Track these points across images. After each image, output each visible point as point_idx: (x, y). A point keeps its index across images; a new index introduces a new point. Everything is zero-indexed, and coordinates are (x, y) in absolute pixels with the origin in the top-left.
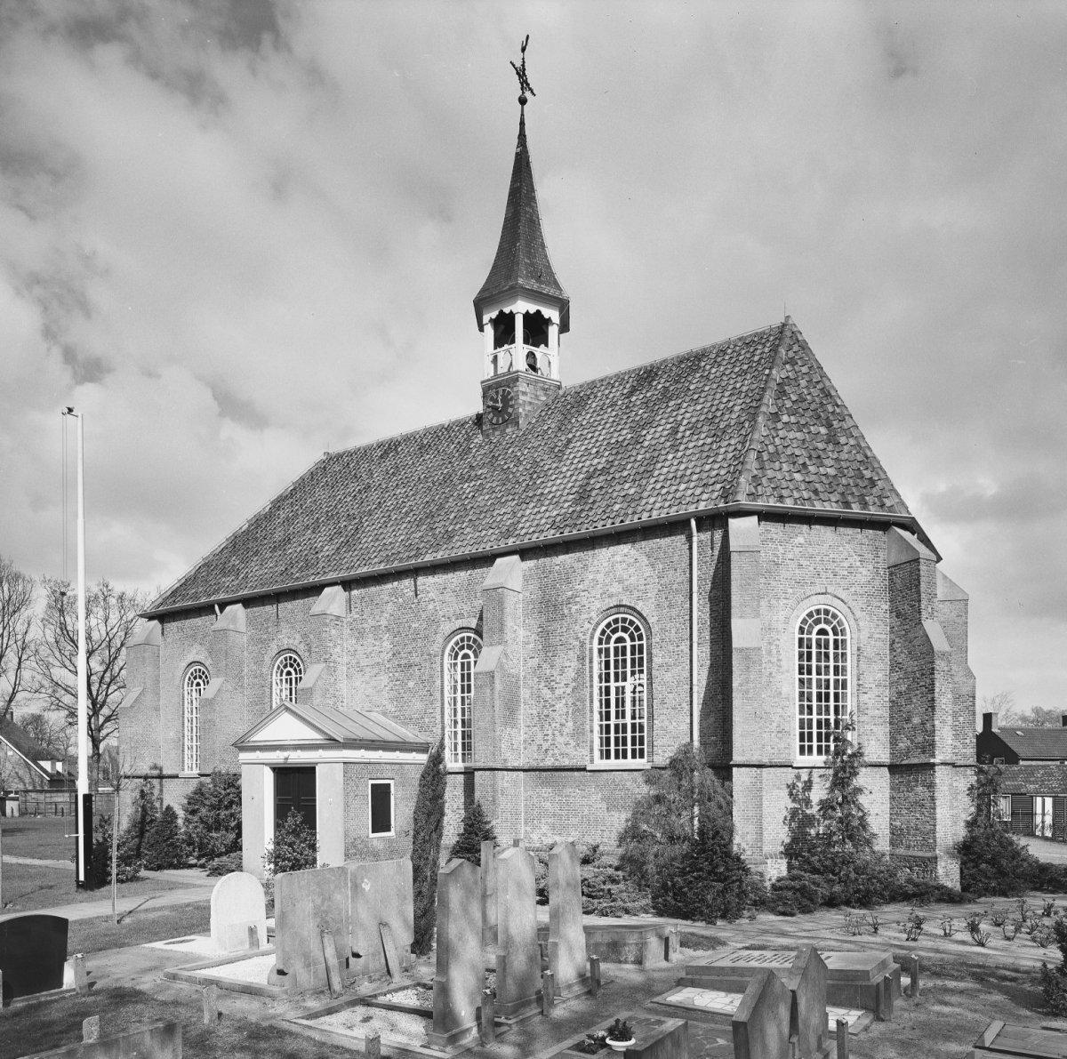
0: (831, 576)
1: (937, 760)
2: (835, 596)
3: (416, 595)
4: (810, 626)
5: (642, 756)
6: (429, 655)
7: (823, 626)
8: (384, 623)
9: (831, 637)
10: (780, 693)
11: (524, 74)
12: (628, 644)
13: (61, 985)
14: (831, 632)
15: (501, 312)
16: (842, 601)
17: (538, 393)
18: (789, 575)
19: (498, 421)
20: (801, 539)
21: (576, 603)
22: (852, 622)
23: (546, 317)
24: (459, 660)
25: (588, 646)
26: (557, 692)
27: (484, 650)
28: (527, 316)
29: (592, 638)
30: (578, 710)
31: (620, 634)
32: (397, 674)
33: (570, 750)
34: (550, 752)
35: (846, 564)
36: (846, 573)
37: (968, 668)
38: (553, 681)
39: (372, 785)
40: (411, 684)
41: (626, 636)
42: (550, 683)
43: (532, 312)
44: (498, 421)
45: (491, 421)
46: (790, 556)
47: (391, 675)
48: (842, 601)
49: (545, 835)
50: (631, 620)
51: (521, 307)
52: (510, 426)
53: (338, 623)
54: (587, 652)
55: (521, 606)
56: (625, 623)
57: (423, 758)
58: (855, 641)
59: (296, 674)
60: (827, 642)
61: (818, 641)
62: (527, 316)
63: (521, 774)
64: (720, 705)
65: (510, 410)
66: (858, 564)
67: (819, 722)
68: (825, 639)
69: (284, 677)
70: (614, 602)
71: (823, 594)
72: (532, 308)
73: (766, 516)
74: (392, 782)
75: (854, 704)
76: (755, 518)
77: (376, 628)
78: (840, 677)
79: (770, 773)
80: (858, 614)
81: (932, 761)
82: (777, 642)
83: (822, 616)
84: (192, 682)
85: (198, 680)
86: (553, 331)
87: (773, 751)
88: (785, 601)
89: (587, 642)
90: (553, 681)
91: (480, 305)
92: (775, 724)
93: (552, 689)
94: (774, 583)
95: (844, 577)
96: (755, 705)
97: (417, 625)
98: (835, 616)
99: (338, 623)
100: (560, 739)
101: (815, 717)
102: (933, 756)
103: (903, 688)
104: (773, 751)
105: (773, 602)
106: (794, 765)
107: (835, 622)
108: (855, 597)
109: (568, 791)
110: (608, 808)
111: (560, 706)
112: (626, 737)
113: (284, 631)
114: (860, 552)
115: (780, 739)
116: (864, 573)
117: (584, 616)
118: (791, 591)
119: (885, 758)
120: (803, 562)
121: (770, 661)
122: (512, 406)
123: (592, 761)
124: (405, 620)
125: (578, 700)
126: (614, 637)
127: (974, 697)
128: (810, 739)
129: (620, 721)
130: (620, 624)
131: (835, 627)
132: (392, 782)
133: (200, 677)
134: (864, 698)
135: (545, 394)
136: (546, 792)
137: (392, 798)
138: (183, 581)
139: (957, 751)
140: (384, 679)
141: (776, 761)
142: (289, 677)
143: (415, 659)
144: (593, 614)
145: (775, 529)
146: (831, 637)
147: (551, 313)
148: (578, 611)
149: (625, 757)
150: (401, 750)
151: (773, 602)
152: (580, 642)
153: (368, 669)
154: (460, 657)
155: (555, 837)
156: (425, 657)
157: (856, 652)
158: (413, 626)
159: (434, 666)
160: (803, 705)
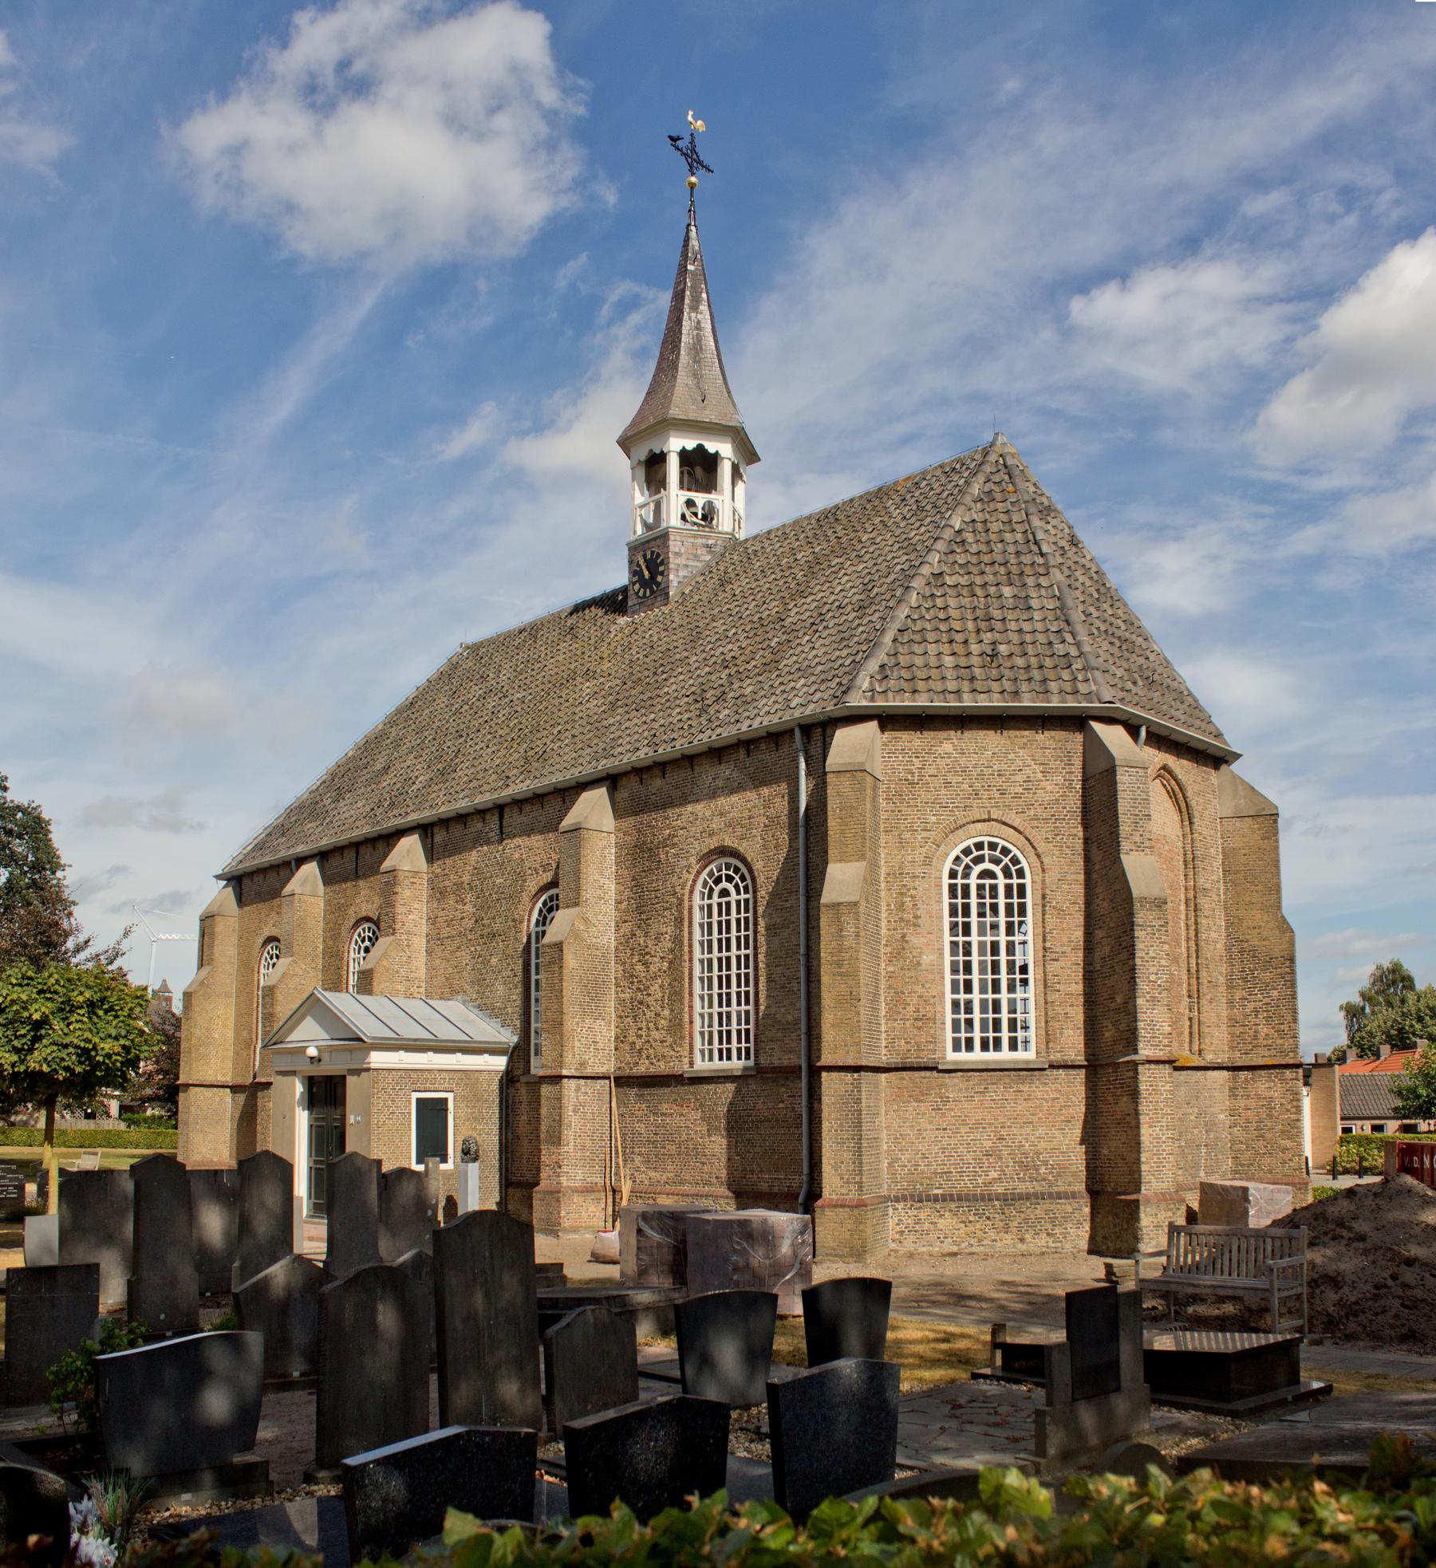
0: (997, 795)
1: (565, 1072)
2: (1004, 823)
4: (967, 867)
6: (514, 920)
7: (987, 865)
8: (466, 878)
9: (1001, 882)
10: (919, 964)
11: (693, 150)
14: (1000, 874)
16: (1015, 829)
17: (699, 552)
18: (931, 797)
19: (645, 593)
20: (948, 747)
21: (674, 845)
22: (1034, 859)
24: (716, 899)
25: (686, 904)
26: (652, 968)
27: (380, 940)
28: (684, 455)
29: (691, 892)
30: (675, 993)
35: (1020, 778)
36: (1020, 790)
37: (1283, 917)
38: (647, 954)
39: (419, 1100)
41: (997, 869)
42: (644, 955)
44: (645, 593)
45: (637, 593)
46: (932, 771)
47: (473, 949)
48: (1015, 829)
49: (638, 1169)
51: (676, 444)
52: (659, 599)
53: (415, 880)
54: (686, 913)
55: (613, 851)
57: (500, 1063)
58: (1038, 886)
59: (738, 893)
60: (994, 888)
61: (980, 887)
62: (684, 455)
63: (1225, 1073)
65: (659, 578)
66: (1040, 775)
69: (716, 899)
70: (713, 843)
71: (984, 821)
72: (691, 444)
73: (889, 720)
74: (450, 1096)
75: (1038, 976)
76: (874, 724)
77: (459, 885)
78: (961, 939)
79: (903, 1079)
80: (1042, 847)
81: (1133, 1057)
82: (912, 892)
84: (711, 890)
85: (724, 884)
86: (725, 470)
87: (908, 1046)
88: (925, 834)
89: (686, 897)
90: (647, 954)
91: (626, 443)
92: (911, 1008)
93: (646, 964)
94: (906, 810)
95: (1017, 796)
96: (852, 983)
98: (1005, 851)
99: (415, 880)
100: (656, 1035)
102: (1136, 1051)
104: (908, 1046)
105: (907, 835)
106: (940, 1067)
108: (1036, 823)
109: (665, 1107)
110: (708, 1131)
111: (655, 988)
113: (363, 893)
114: (1041, 760)
115: (919, 1028)
116: (1049, 788)
117: (684, 863)
118: (934, 819)
119: (609, 1067)
120: (953, 779)
121: (902, 919)
122: (662, 574)
123: (691, 1064)
124: (488, 875)
125: (675, 980)
126: (977, 869)
127: (1292, 960)
131: (1006, 866)
132: (450, 1096)
133: (730, 879)
134: (1052, 967)
135: (710, 552)
136: (639, 1108)
137: (450, 1117)
138: (271, 829)
139: (1270, 1042)
140: (465, 956)
141: (912, 1060)
142: (724, 900)
143: (497, 926)
144: (693, 860)
145: (911, 740)
146: (1001, 882)
147: (724, 449)
148: (676, 855)
149: (729, 1058)
150: (467, 1051)
151: (907, 835)
152: (678, 899)
154: (715, 895)
156: (510, 923)
157: (1039, 902)
158: (498, 881)
160: (958, 981)
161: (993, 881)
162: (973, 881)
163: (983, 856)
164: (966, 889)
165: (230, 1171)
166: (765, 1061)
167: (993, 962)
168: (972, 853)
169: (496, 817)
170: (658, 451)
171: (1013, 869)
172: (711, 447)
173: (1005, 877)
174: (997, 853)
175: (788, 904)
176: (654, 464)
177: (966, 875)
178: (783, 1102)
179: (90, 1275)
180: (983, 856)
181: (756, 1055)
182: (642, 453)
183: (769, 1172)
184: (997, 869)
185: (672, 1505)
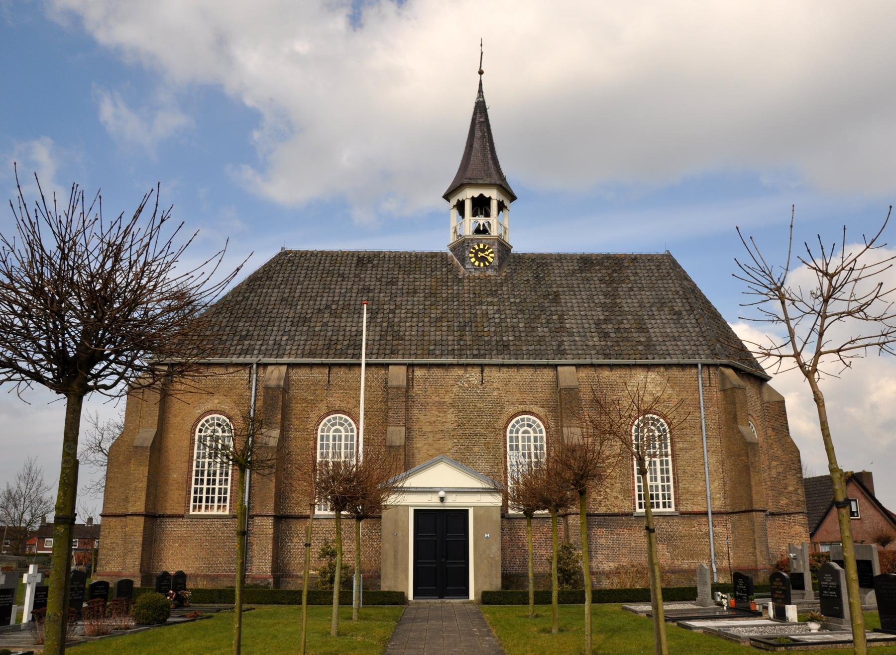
3: (482, 383)
5: (669, 507)
9: (532, 435)
12: (343, 434)
13: (9, 624)
15: (458, 200)
23: (487, 196)
28: (473, 199)
31: (337, 427)
32: (462, 441)
33: (618, 503)
34: (603, 504)
40: (476, 449)
43: (476, 196)
50: (350, 423)
56: (202, 430)
60: (529, 438)
61: (523, 438)
64: (722, 475)
67: (208, 490)
68: (339, 435)
83: (207, 425)
97: (482, 405)
101: (205, 486)
103: (781, 470)
107: (534, 426)
112: (207, 494)
126: (522, 430)
128: (207, 498)
129: (654, 484)
130: (338, 421)
147: (492, 194)
153: (431, 435)
154: (520, 432)
155: (609, 563)
158: (478, 405)
159: (498, 437)
161: (340, 434)
162: (520, 435)
163: (344, 425)
164: (517, 438)
165: (797, 608)
166: (683, 509)
167: (323, 441)
168: (202, 430)
169: (327, 371)
170: (461, 200)
171: (537, 429)
172: (487, 193)
173: (346, 432)
174: (204, 429)
175: (693, 440)
176: (460, 206)
177: (328, 431)
178: (694, 527)
179: (212, 444)
180: (344, 425)
181: (676, 505)
182: (454, 201)
183: (688, 560)
184: (530, 430)
185: (85, 393)
